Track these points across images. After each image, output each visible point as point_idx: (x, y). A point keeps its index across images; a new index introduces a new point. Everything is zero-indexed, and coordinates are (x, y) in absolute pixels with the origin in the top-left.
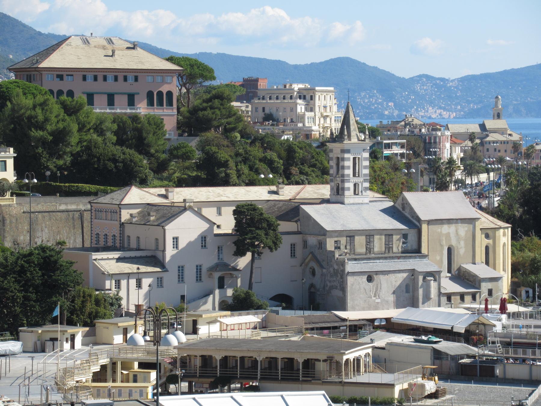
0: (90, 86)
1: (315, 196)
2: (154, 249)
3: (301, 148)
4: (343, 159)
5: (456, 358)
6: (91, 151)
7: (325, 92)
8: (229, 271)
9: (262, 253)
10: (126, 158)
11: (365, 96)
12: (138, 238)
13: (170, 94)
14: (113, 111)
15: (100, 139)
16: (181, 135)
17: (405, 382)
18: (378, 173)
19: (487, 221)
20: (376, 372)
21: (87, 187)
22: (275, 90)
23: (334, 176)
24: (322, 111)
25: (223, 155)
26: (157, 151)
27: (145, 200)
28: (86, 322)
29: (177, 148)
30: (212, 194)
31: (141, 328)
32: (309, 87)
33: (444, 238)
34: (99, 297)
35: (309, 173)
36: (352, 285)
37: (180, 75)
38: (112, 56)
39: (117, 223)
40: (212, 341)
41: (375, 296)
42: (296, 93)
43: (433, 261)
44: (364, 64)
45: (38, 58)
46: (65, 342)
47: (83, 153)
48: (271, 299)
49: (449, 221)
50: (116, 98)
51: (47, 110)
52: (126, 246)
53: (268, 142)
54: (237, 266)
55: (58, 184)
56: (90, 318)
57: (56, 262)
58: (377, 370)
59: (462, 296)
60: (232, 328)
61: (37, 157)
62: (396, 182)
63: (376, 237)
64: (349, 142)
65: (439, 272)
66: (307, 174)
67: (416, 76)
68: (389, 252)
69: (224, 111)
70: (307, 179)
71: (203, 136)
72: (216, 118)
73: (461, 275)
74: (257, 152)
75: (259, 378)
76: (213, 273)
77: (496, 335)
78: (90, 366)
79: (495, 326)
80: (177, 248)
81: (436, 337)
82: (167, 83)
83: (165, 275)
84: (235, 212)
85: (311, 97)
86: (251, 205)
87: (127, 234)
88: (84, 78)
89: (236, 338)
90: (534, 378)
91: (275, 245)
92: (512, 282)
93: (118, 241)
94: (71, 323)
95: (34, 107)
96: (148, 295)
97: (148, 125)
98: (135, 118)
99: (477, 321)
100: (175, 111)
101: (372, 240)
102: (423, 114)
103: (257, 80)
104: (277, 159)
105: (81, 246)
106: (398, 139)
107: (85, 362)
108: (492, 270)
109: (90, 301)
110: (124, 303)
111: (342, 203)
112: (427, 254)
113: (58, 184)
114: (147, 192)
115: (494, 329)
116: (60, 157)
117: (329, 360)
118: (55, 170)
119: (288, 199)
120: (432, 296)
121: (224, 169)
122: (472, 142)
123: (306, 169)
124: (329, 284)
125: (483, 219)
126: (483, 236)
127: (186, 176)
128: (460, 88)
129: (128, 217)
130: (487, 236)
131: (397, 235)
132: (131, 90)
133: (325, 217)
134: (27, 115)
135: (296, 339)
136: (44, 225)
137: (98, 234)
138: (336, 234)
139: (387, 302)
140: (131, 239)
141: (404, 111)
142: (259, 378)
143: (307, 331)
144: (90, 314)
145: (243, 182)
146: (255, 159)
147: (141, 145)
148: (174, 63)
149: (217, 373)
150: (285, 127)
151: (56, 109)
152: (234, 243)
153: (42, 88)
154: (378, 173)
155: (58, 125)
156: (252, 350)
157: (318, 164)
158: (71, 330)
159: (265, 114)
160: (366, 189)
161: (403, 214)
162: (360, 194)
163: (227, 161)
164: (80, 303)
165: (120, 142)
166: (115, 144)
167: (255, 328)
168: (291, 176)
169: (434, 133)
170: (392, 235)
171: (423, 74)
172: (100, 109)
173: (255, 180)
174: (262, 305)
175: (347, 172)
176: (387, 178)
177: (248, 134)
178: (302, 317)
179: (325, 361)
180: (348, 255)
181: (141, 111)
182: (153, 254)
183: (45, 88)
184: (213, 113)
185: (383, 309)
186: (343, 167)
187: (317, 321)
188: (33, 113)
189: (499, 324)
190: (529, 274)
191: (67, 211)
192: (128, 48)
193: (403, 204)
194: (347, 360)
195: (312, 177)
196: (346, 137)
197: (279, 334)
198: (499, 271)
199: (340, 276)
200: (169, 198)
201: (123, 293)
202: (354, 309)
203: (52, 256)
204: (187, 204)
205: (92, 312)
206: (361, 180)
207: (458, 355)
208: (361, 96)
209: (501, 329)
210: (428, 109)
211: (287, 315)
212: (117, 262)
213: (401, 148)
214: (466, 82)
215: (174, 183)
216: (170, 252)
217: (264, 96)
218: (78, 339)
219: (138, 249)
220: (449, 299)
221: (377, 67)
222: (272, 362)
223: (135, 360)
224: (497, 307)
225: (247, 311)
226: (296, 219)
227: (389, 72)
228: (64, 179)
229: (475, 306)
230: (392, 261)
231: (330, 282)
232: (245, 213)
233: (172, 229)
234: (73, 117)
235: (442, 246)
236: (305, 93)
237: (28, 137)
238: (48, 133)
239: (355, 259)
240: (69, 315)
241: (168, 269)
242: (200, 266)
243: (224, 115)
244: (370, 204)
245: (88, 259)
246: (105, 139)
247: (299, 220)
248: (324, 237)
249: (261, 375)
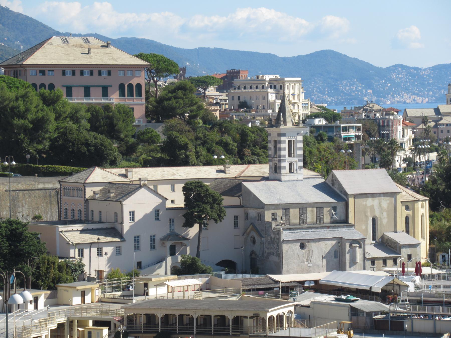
0: (69, 80)
1: (258, 174)
3: (253, 133)
4: (280, 142)
5: (370, 314)
6: (67, 136)
7: (293, 82)
8: (180, 240)
9: (207, 224)
10: (97, 143)
11: (346, 84)
12: (100, 212)
13: (139, 86)
14: (89, 101)
15: (75, 126)
16: (149, 122)
17: (321, 336)
18: (323, 153)
19: (407, 194)
20: (298, 327)
21: (62, 168)
22: (249, 80)
23: (272, 156)
24: (291, 99)
25: (183, 139)
26: (126, 136)
27: (107, 179)
28: (50, 286)
29: (143, 134)
30: (166, 173)
31: (97, 291)
32: (279, 77)
33: (369, 210)
34: (62, 264)
35: (260, 154)
36: (287, 252)
37: (149, 70)
38: (88, 54)
39: (82, 199)
40: (158, 301)
41: (307, 261)
42: (267, 83)
43: (359, 230)
44: (345, 55)
45: (23, 56)
46: (29, 304)
47: (59, 139)
48: (217, 264)
49: (373, 195)
50: (92, 90)
51: (27, 101)
52: (90, 219)
53: (226, 128)
54: (188, 235)
55: (37, 166)
56: (53, 282)
57: (21, 234)
58: (299, 326)
59: (385, 261)
60: (180, 290)
61: (19, 143)
62: (339, 161)
63: (309, 210)
64: (285, 127)
65: (364, 240)
66: (258, 155)
67: (392, 66)
68: (320, 222)
69: (186, 101)
70: (258, 159)
71: (167, 123)
72: (179, 107)
73: (384, 242)
74: (215, 136)
75: (195, 333)
76: (165, 242)
77: (409, 294)
78: (46, 324)
79: (408, 286)
80: (133, 220)
81: (354, 296)
82: (136, 77)
83: (123, 245)
84: (184, 189)
85: (281, 86)
86: (198, 183)
87: (91, 208)
88: (64, 73)
89: (180, 298)
90: (438, 331)
91: (220, 217)
92: (430, 248)
93: (83, 215)
94: (36, 287)
95: (17, 99)
96: (109, 260)
97: (118, 113)
98: (107, 108)
99: (392, 282)
100: (144, 101)
101: (304, 212)
102: (398, 100)
103: (239, 72)
104: (231, 142)
105: (57, 220)
106: (355, 123)
107: (43, 320)
108: (412, 237)
109: (54, 268)
110: (86, 269)
111: (280, 180)
112: (353, 223)
113: (37, 166)
115: (408, 289)
116: (39, 142)
117: (256, 317)
118: (35, 153)
119: (234, 177)
120: (358, 260)
121: (184, 151)
122: (425, 125)
123: (258, 150)
124: (267, 251)
125: (403, 193)
126: (404, 207)
127: (150, 158)
128: (432, 76)
129: (92, 194)
130: (407, 208)
131: (327, 207)
132: (105, 83)
133: (262, 192)
134: (10, 106)
135: (234, 299)
136: (24, 202)
137: (66, 209)
138: (273, 208)
139: (318, 266)
140: (94, 213)
141: (381, 97)
142: (195, 333)
143: (244, 293)
144: (54, 279)
145: (201, 162)
146: (212, 142)
147: (112, 131)
148: (143, 59)
149: (158, 330)
150: (257, 113)
151: (35, 100)
152: (183, 216)
153: (25, 82)
154: (323, 153)
155: (37, 114)
156: (188, 308)
158: (37, 293)
159: (240, 102)
160: (300, 168)
161: (332, 189)
162: (295, 172)
163: (187, 144)
164: (44, 269)
165: (94, 128)
166: (89, 131)
167: (198, 290)
168: (244, 157)
169: (387, 117)
170: (323, 208)
171: (399, 64)
172: (78, 100)
173: (211, 161)
174: (206, 270)
175: (283, 153)
176: (331, 158)
177: (210, 121)
178: (241, 280)
179: (251, 318)
180: (283, 225)
181: (114, 101)
183: (29, 82)
184: (177, 103)
185: (314, 272)
186: (280, 149)
187: (253, 283)
188: (16, 104)
189: (412, 284)
190: (445, 240)
191: (45, 189)
192: (102, 46)
193: (333, 181)
194: (271, 317)
195: (263, 157)
196: (282, 123)
197: (219, 295)
198: (418, 239)
199: (277, 243)
200: (129, 177)
201: (85, 261)
202: (288, 273)
203: (18, 229)
204: (142, 182)
205: (56, 277)
206: (296, 160)
207: (373, 312)
208: (342, 84)
209: (414, 289)
210: (403, 95)
211: (229, 278)
212: (80, 233)
213: (357, 130)
214: (437, 70)
215: (141, 163)
216: (127, 225)
217: (239, 87)
218: (41, 301)
219: (100, 222)
220: (373, 263)
221: (357, 58)
222: (207, 319)
223: (90, 318)
224: (414, 269)
225: (192, 275)
226: (238, 194)
227: (368, 63)
228: (42, 161)
229: (395, 269)
230: (323, 230)
231: (268, 249)
232: (192, 189)
233: (129, 204)
234: (52, 107)
235: (367, 217)
236: (275, 83)
237: (12, 125)
238: (29, 122)
239: (290, 229)
240: (34, 280)
241: (126, 239)
242: (154, 236)
243: (187, 104)
244: (304, 180)
245: (55, 231)
246: (80, 126)
247: (241, 195)
249: (197, 331)
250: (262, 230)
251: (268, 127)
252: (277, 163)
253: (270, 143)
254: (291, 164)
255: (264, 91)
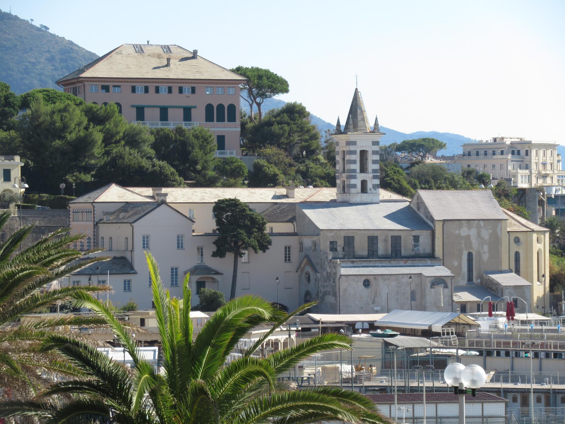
2: (124, 249)
12: (111, 238)
23: (340, 172)
27: (124, 198)
30: (208, 195)
33: (463, 242)
85: (527, 151)
87: (100, 235)
88: (134, 90)
114: (132, 192)
153: (76, 98)
157: (393, 183)
161: (417, 214)
182: (123, 255)
193: (418, 204)
231: (324, 287)
236: (519, 147)
248: (317, 237)
250: (318, 264)
251: (335, 134)
252: (345, 180)
253: (338, 154)
254: (364, 183)
255: (503, 158)
